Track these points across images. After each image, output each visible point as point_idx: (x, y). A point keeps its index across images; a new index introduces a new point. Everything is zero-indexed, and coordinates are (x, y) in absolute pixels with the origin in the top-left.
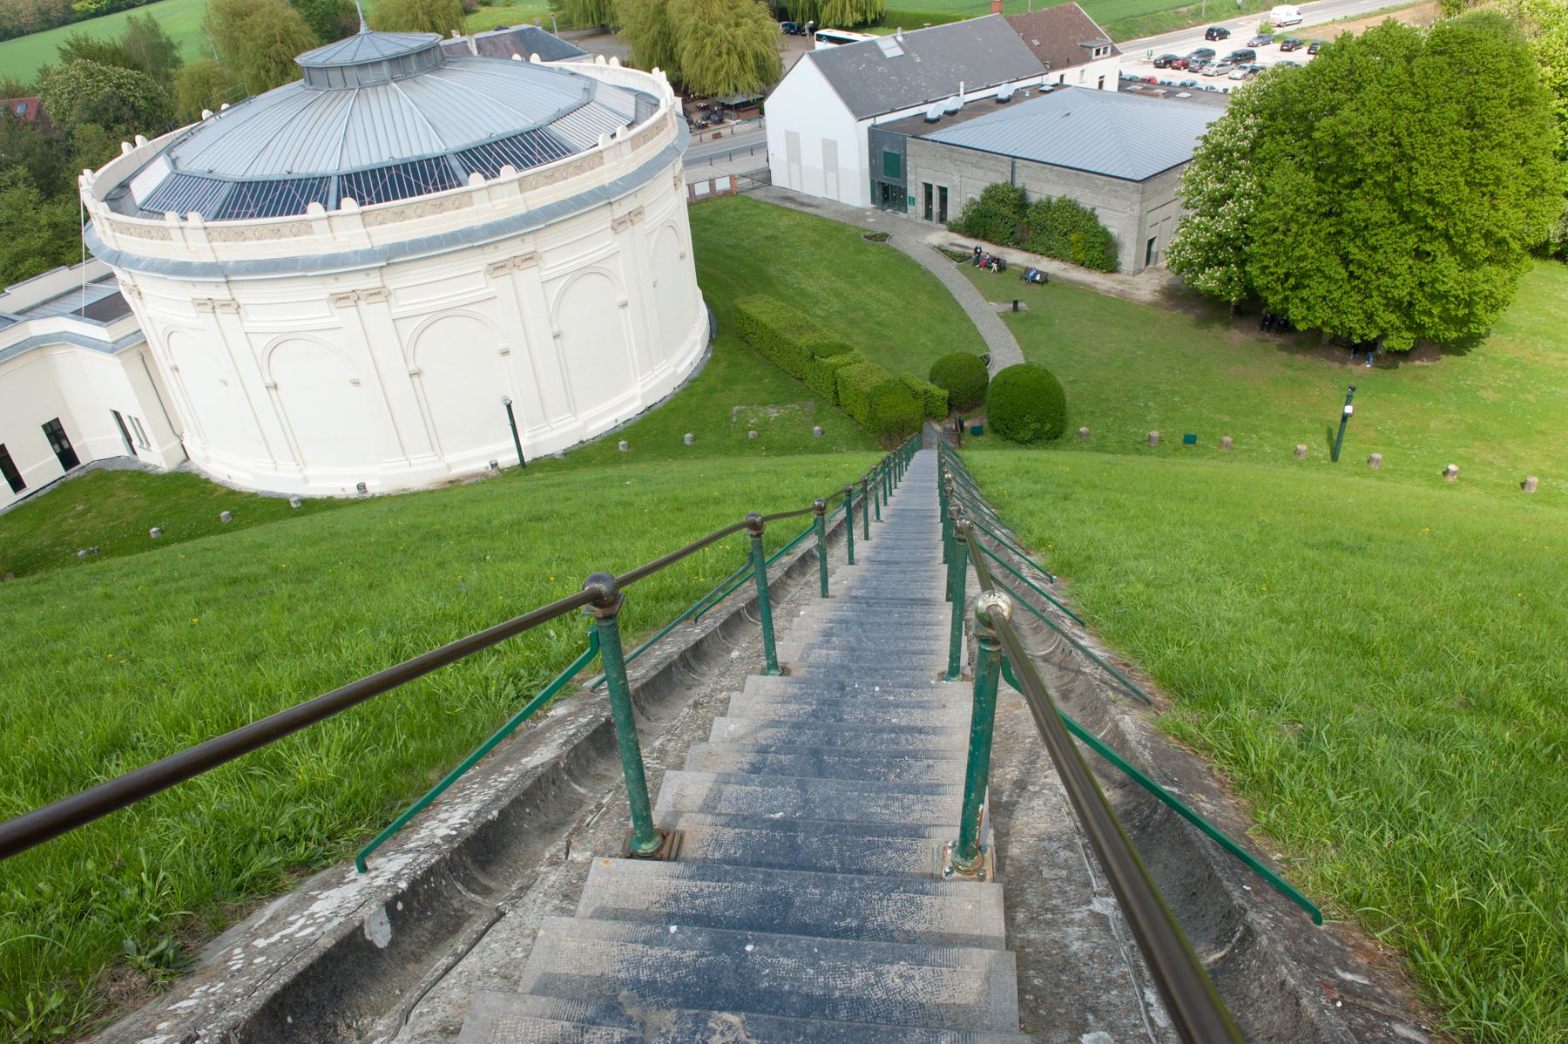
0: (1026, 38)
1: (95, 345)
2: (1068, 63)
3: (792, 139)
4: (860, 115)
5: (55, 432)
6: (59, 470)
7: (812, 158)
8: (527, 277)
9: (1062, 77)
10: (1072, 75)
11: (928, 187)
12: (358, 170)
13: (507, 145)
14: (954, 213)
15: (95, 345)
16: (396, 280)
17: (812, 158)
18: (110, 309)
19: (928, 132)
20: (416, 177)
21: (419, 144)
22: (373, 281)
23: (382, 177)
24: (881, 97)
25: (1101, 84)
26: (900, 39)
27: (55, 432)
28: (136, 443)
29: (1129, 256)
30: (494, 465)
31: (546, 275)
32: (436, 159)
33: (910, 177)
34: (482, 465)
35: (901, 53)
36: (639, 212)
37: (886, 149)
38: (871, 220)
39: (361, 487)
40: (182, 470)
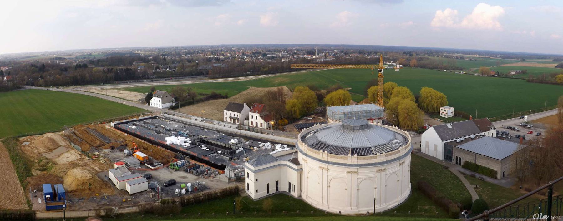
0: (477, 125)
1: (294, 169)
3: (427, 143)
4: (443, 140)
5: (277, 183)
6: (275, 191)
7: (431, 148)
10: (486, 133)
11: (457, 157)
12: (355, 147)
14: (462, 164)
15: (294, 169)
17: (431, 148)
19: (457, 146)
20: (366, 151)
21: (366, 144)
23: (359, 149)
24: (447, 137)
25: (492, 135)
26: (451, 124)
27: (277, 183)
28: (291, 190)
29: (499, 176)
30: (368, 213)
31: (387, 173)
32: (369, 148)
33: (453, 155)
34: (365, 212)
35: (452, 127)
36: (404, 162)
37: (448, 148)
38: (444, 163)
39: (340, 212)
40: (299, 199)
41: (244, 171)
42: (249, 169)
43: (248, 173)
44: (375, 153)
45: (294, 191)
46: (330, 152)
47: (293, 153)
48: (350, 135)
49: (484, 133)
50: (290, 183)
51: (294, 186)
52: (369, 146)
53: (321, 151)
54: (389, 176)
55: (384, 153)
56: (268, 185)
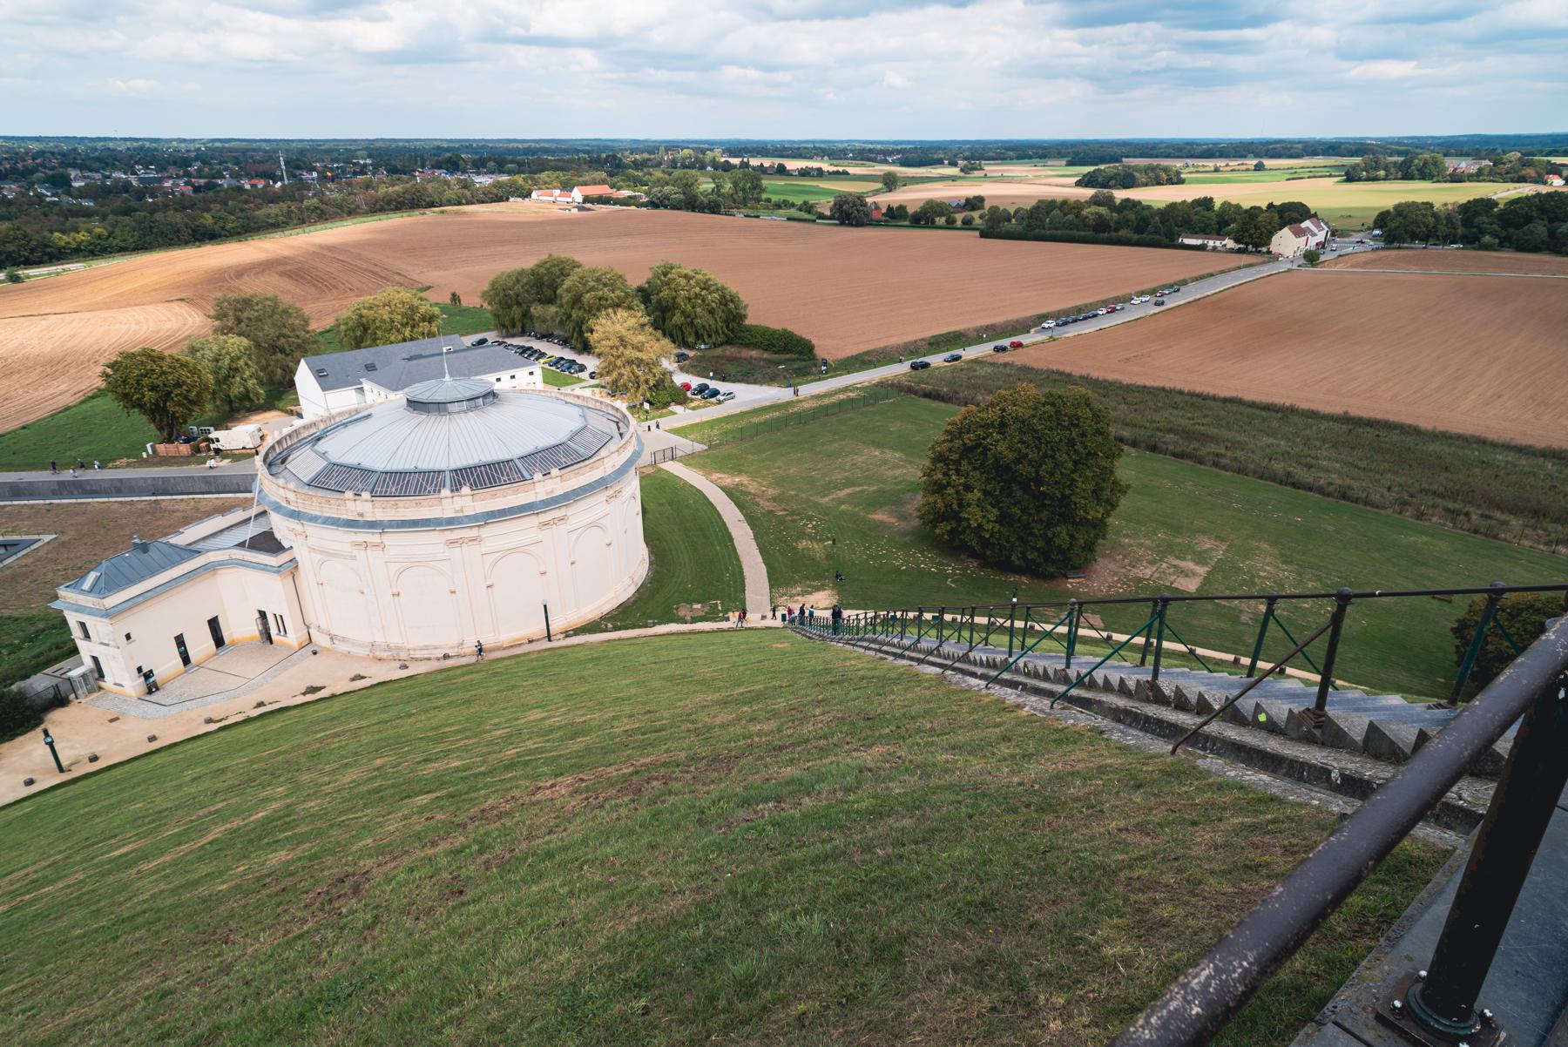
5: (214, 624)
8: (562, 529)
13: (491, 469)
15: (265, 568)
16: (486, 532)
18: (267, 543)
22: (474, 533)
27: (214, 624)
31: (484, 550)
41: (64, 622)
42: (80, 609)
43: (83, 625)
44: (527, 475)
45: (282, 633)
46: (386, 492)
47: (250, 519)
48: (439, 427)
50: (263, 615)
51: (280, 620)
52: (507, 457)
53: (349, 494)
54: (578, 538)
55: (555, 472)
56: (180, 641)
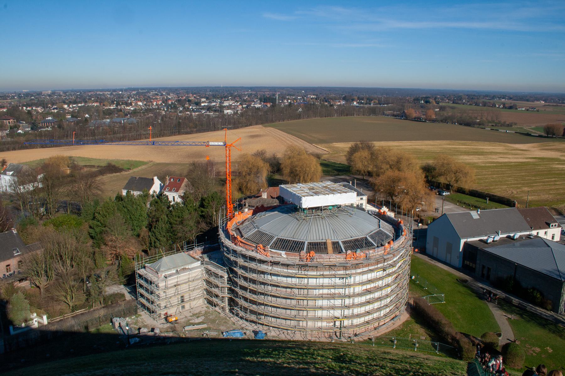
2: (540, 228)
9: (538, 233)
49: (546, 230)
